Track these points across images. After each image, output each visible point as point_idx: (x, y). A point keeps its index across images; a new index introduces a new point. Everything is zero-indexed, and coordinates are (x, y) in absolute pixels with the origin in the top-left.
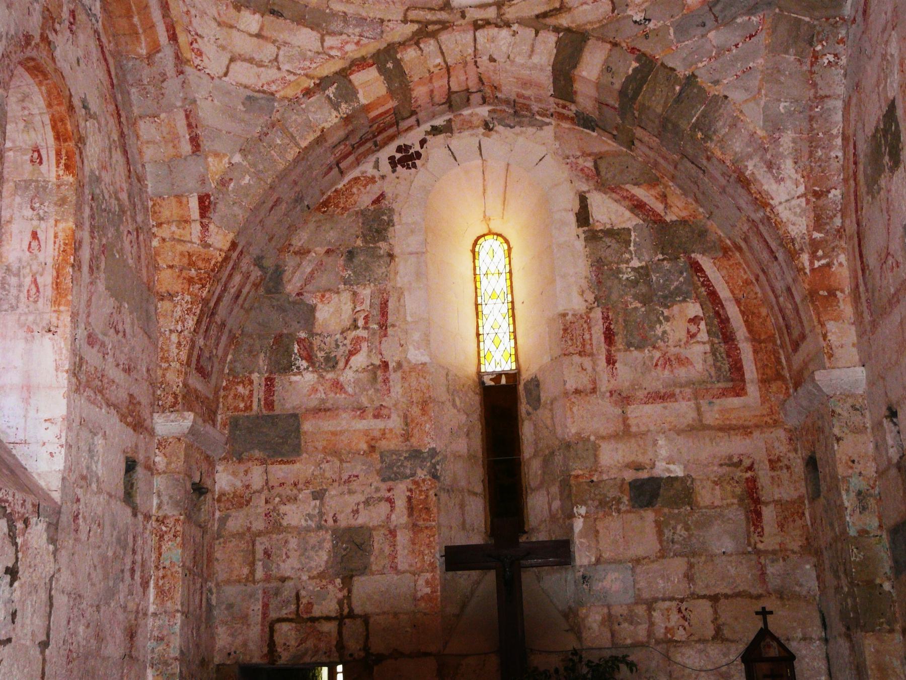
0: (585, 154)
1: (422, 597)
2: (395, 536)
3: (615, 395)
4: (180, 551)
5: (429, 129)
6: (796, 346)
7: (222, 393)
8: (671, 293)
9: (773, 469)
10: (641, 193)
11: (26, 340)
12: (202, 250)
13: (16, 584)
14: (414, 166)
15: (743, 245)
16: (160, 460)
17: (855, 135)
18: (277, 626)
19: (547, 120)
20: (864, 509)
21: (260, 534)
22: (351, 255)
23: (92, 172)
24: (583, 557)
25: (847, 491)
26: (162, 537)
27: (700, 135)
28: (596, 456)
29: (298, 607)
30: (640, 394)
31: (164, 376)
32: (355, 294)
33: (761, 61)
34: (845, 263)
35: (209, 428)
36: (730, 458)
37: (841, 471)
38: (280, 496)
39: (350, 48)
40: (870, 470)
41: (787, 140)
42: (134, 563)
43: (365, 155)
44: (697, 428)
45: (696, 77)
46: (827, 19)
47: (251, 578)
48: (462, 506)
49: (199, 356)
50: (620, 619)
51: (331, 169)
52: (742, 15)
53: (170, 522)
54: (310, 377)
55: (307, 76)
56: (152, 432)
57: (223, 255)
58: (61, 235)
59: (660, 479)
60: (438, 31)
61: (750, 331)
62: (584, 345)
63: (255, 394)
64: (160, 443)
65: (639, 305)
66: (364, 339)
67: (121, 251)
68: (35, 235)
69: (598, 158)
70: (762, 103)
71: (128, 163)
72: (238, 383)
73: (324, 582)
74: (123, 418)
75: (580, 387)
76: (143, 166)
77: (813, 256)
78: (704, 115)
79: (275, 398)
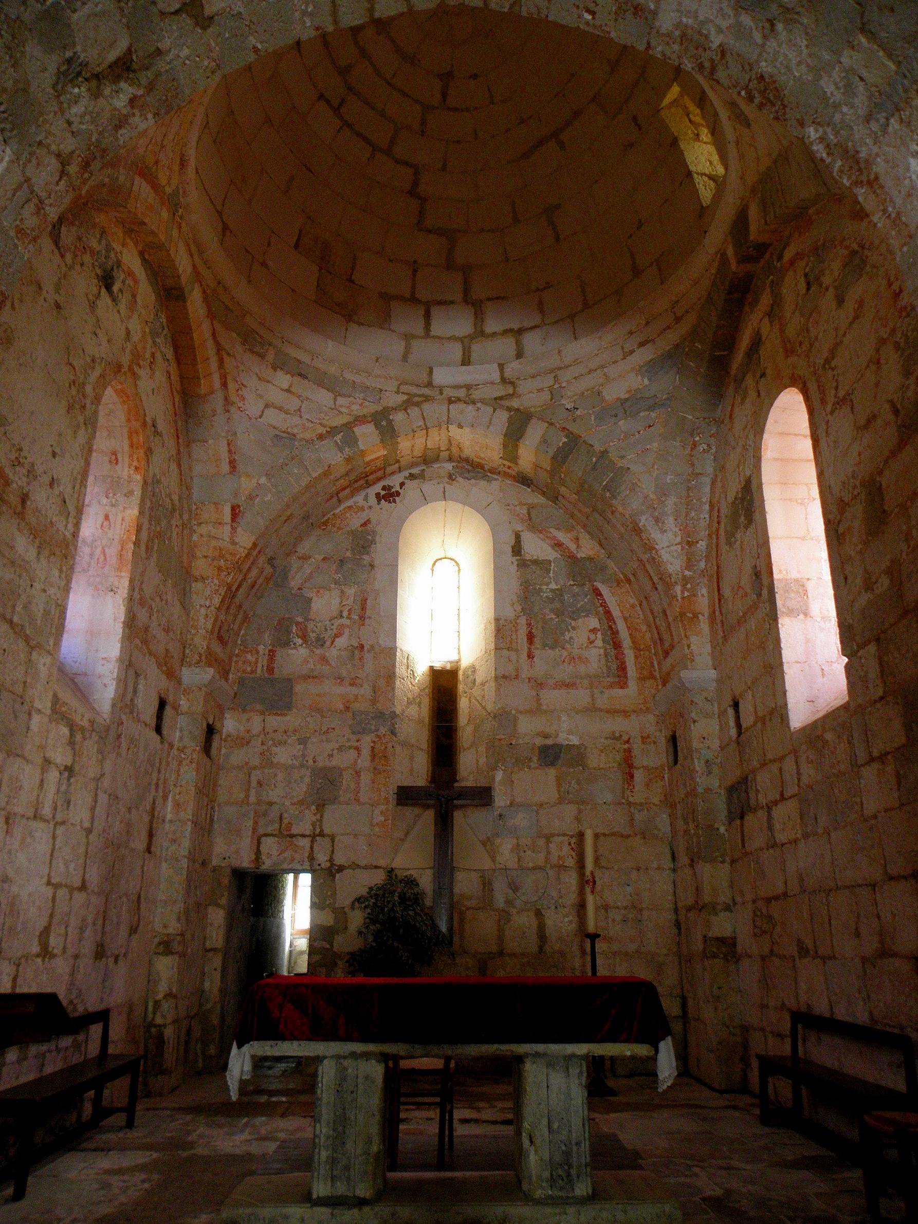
0: (522, 504)
1: (377, 824)
2: (359, 776)
3: (532, 681)
4: (194, 773)
5: (407, 475)
6: (666, 654)
7: (234, 659)
8: (578, 610)
9: (643, 743)
10: (561, 536)
11: (93, 596)
12: (229, 545)
13: (72, 780)
14: (394, 501)
15: (632, 578)
16: (184, 703)
17: (719, 502)
18: (263, 839)
19: (496, 477)
20: (710, 773)
21: (255, 768)
22: (342, 562)
23: (155, 475)
24: (500, 800)
25: (699, 759)
26: (181, 762)
27: (608, 494)
28: (515, 726)
29: (281, 826)
30: (551, 682)
31: (192, 639)
32: (342, 592)
33: (655, 445)
34: (706, 594)
35: (223, 682)
36: (614, 732)
37: (695, 744)
38: (273, 740)
39: (355, 407)
40: (716, 744)
41: (671, 502)
42: (158, 779)
43: (358, 490)
44: (592, 710)
45: (608, 452)
46: (704, 418)
48: (412, 758)
49: (220, 627)
50: (526, 849)
51: (332, 497)
52: (644, 410)
53: (189, 751)
54: (303, 652)
55: (320, 424)
56: (179, 682)
57: (246, 551)
58: (128, 519)
59: (562, 745)
60: (422, 402)
61: (633, 642)
62: (511, 642)
63: (260, 660)
64: (185, 690)
65: (554, 617)
66: (348, 626)
67: (170, 539)
68: (107, 517)
70: (654, 475)
71: (181, 475)
72: (247, 652)
73: (303, 808)
74: (159, 666)
75: (507, 674)
76: (192, 478)
77: (684, 586)
78: (612, 480)
79: (275, 665)
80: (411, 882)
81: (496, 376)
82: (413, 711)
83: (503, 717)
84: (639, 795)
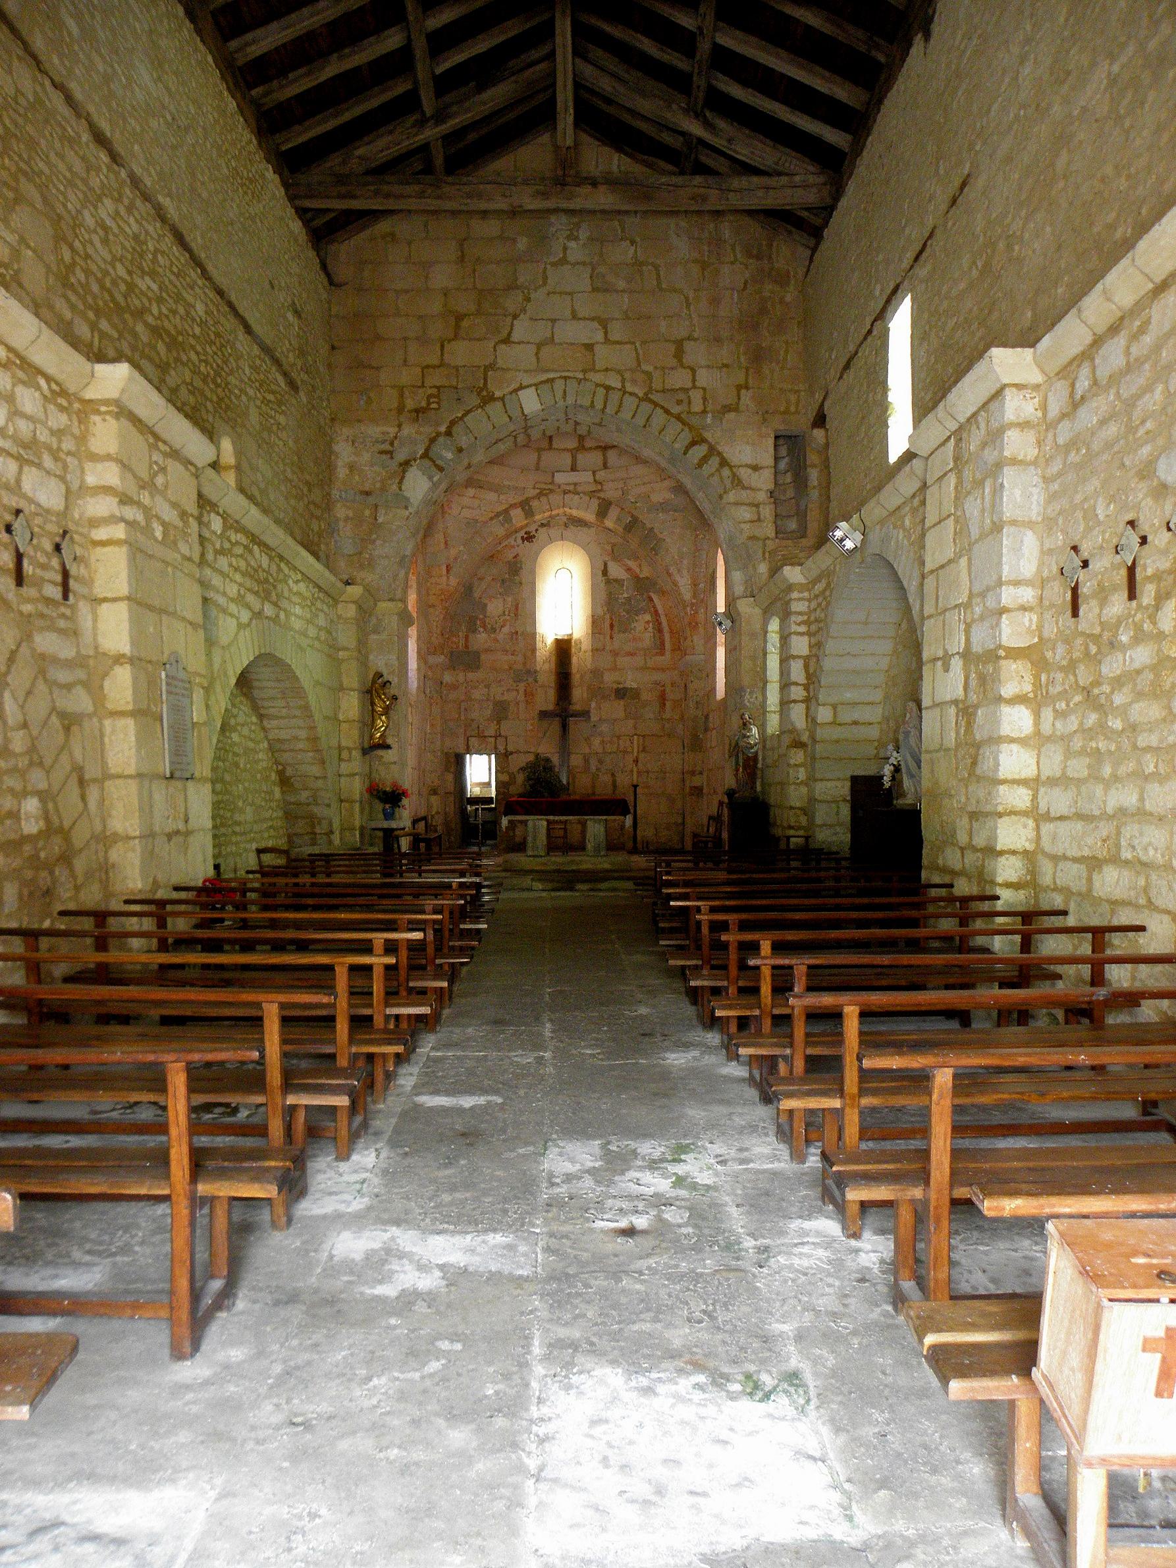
10: (632, 564)
24: (594, 718)
44: (644, 668)
69: (614, 545)
80: (548, 760)
81: (591, 479)
82: (547, 666)
83: (596, 673)
84: (667, 715)
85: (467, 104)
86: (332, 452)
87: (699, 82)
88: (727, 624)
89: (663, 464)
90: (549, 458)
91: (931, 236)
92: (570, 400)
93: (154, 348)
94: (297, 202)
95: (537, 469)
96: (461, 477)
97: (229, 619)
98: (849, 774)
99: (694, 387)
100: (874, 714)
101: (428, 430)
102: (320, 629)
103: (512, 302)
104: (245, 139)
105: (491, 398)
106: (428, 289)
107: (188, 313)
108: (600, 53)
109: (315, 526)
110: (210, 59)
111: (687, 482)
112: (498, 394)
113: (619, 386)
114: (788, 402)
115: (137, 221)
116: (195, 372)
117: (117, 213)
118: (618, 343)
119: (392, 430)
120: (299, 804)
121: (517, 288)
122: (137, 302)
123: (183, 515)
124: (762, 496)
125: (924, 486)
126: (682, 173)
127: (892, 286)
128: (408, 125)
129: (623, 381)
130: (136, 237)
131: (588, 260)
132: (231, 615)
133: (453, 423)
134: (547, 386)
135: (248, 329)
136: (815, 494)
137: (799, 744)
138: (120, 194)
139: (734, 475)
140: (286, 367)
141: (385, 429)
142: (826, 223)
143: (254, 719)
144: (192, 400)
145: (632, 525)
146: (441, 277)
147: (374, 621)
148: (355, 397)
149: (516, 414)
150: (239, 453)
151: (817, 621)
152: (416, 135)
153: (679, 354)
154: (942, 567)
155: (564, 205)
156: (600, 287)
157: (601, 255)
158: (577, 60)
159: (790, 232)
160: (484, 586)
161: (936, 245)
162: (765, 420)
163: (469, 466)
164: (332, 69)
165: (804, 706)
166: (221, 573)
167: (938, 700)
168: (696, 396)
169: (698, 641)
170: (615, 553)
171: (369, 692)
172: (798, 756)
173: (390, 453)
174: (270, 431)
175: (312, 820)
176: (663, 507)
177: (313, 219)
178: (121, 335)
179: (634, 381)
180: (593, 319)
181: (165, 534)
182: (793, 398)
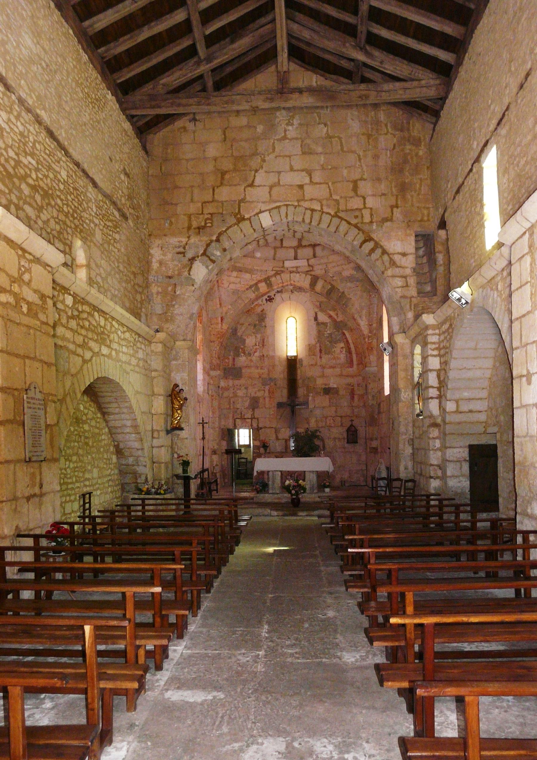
10: (332, 313)
24: (311, 406)
41: (364, 312)
44: (341, 375)
47: (229, 408)
54: (244, 358)
69: (321, 303)
81: (306, 264)
85: (225, 51)
86: (149, 254)
87: (362, 29)
88: (389, 349)
89: (348, 254)
90: (281, 253)
91: (507, 109)
92: (290, 218)
93: (33, 198)
94: (128, 112)
95: (274, 259)
96: (226, 266)
97: (77, 358)
98: (467, 444)
99: (365, 207)
100: (482, 406)
101: (205, 239)
102: (139, 359)
103: (254, 163)
104: (93, 77)
105: (243, 219)
106: (205, 158)
107: (55, 177)
108: (302, 16)
109: (138, 297)
110: (71, 32)
111: (363, 264)
112: (247, 216)
113: (319, 208)
114: (423, 215)
115: (22, 124)
116: (60, 210)
117: (9, 120)
118: (317, 183)
119: (184, 240)
120: (128, 465)
121: (258, 154)
122: (22, 171)
123: (43, 297)
124: (408, 271)
125: (510, 263)
126: (354, 83)
127: (484, 141)
128: (190, 65)
129: (322, 206)
130: (21, 134)
131: (299, 136)
132: (78, 355)
133: (220, 234)
134: (275, 211)
135: (95, 185)
136: (441, 269)
137: (435, 425)
138: (11, 109)
139: (391, 259)
140: (120, 206)
141: (181, 239)
142: (442, 108)
143: (99, 415)
144: (58, 228)
145: (331, 291)
146: (212, 151)
147: (174, 352)
148: (162, 222)
149: (257, 226)
150: (89, 257)
151: (444, 347)
152: (195, 70)
153: (355, 189)
154: (524, 316)
155: (283, 105)
156: (307, 152)
157: (307, 133)
158: (289, 21)
159: (420, 115)
160: (243, 329)
161: (511, 115)
162: (409, 226)
163: (231, 259)
164: (145, 34)
165: (437, 401)
166: (71, 330)
167: (524, 403)
168: (366, 214)
169: (373, 358)
170: (321, 307)
171: (170, 396)
172: (435, 432)
173: (183, 253)
174: (109, 243)
175: (136, 475)
176: (350, 279)
177: (137, 121)
178: (11, 191)
179: (328, 206)
180: (303, 170)
181: (29, 310)
182: (426, 212)
